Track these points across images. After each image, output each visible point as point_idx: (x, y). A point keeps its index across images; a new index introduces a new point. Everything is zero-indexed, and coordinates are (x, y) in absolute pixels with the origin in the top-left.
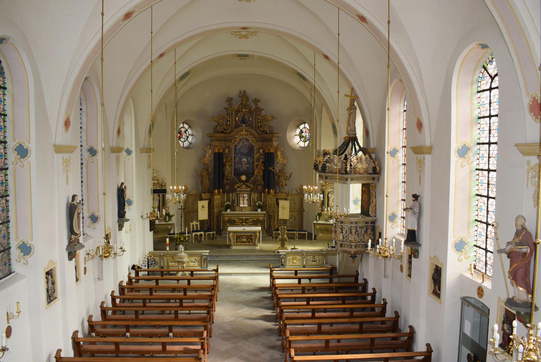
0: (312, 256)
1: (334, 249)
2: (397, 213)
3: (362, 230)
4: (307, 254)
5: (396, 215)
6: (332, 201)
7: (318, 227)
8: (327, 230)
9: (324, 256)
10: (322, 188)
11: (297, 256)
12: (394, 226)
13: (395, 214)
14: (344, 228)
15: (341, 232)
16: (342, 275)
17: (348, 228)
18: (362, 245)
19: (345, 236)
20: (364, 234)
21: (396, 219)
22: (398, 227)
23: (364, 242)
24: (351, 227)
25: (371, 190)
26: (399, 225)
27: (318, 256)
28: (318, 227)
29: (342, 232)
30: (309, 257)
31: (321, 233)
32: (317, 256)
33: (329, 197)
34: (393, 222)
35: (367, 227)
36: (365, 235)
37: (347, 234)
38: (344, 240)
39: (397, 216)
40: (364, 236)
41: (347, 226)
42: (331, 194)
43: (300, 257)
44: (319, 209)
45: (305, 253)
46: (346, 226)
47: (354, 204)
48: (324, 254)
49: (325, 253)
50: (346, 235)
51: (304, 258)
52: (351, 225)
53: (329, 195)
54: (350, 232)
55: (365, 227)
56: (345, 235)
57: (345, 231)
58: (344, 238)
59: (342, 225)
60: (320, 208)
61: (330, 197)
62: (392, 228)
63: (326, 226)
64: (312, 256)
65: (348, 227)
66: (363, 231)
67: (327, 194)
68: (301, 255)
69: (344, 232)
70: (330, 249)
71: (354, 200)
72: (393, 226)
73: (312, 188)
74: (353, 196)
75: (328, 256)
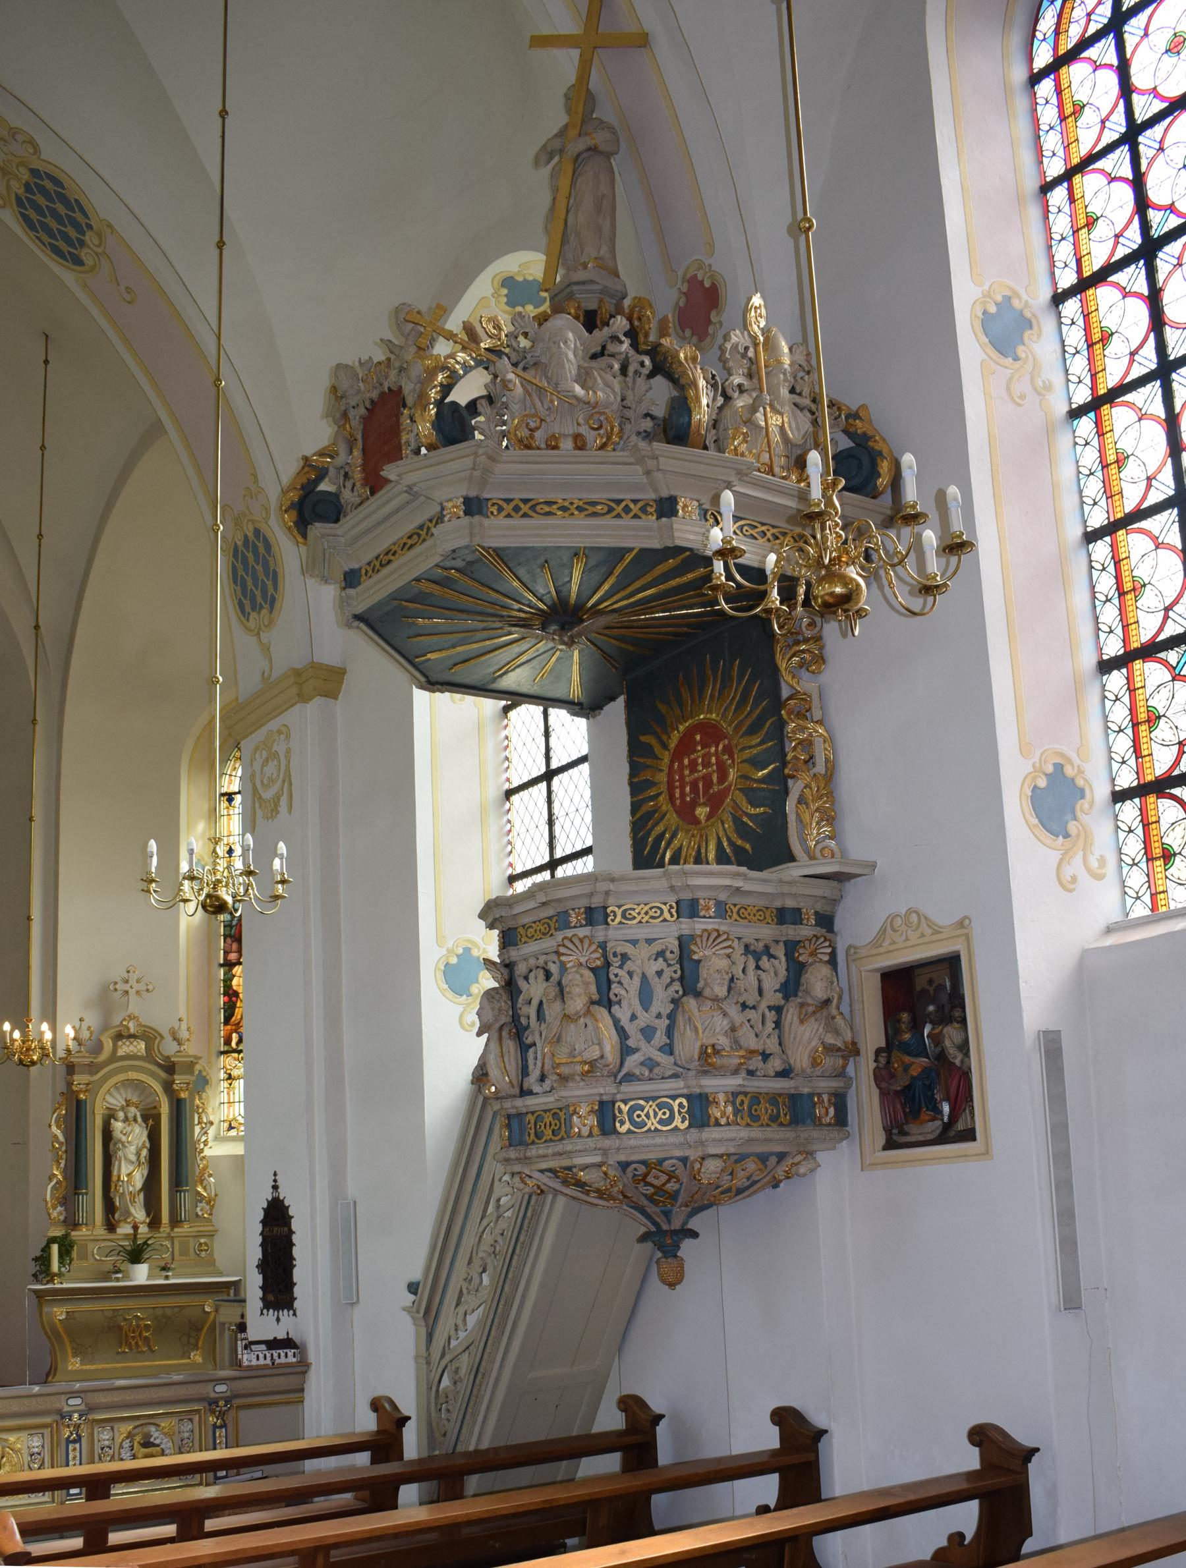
0: (129, 1427)
1: (283, 1360)
2: (1081, 772)
3: (763, 976)
4: (91, 1409)
5: (1080, 782)
6: (133, 1158)
7: (59, 1313)
8: (120, 1328)
9: (222, 1415)
10: (70, 1084)
11: (12, 1438)
12: (1075, 866)
13: (1069, 771)
14: (625, 957)
15: (596, 997)
16: (484, 1445)
17: (661, 954)
18: (773, 1099)
19: (631, 1029)
20: (778, 1010)
21: (1079, 814)
22: (1100, 877)
23: (785, 1073)
24: (684, 942)
25: (783, 666)
26: (1102, 862)
27: (174, 1421)
28: (59, 1313)
29: (605, 1000)
30: (106, 1436)
31: (75, 1355)
32: (164, 1424)
33: (117, 1134)
34: (1067, 836)
35: (791, 947)
36: (791, 1014)
37: (654, 1009)
38: (632, 1062)
39: (1083, 797)
40: (778, 1024)
41: (649, 941)
42: (126, 1120)
43: (36, 1442)
44: (55, 1214)
45: (78, 1401)
46: (634, 942)
47: (450, 994)
48: (213, 1402)
49: (221, 1388)
50: (644, 1018)
51: (68, 1441)
52: (686, 926)
53: (118, 1126)
54: (677, 986)
55: (780, 951)
56: (634, 1017)
57: (637, 981)
58: (626, 1051)
59: (600, 933)
60: (59, 1208)
61: (124, 1138)
62: (1068, 885)
63: (107, 1305)
64: (129, 1427)
65: (657, 947)
66: (771, 983)
67: (99, 1122)
68: (47, 1420)
69: (627, 990)
70: (262, 1362)
71: (447, 965)
72: (1068, 872)
73: (17, 1035)
74: (440, 939)
75: (243, 1414)
